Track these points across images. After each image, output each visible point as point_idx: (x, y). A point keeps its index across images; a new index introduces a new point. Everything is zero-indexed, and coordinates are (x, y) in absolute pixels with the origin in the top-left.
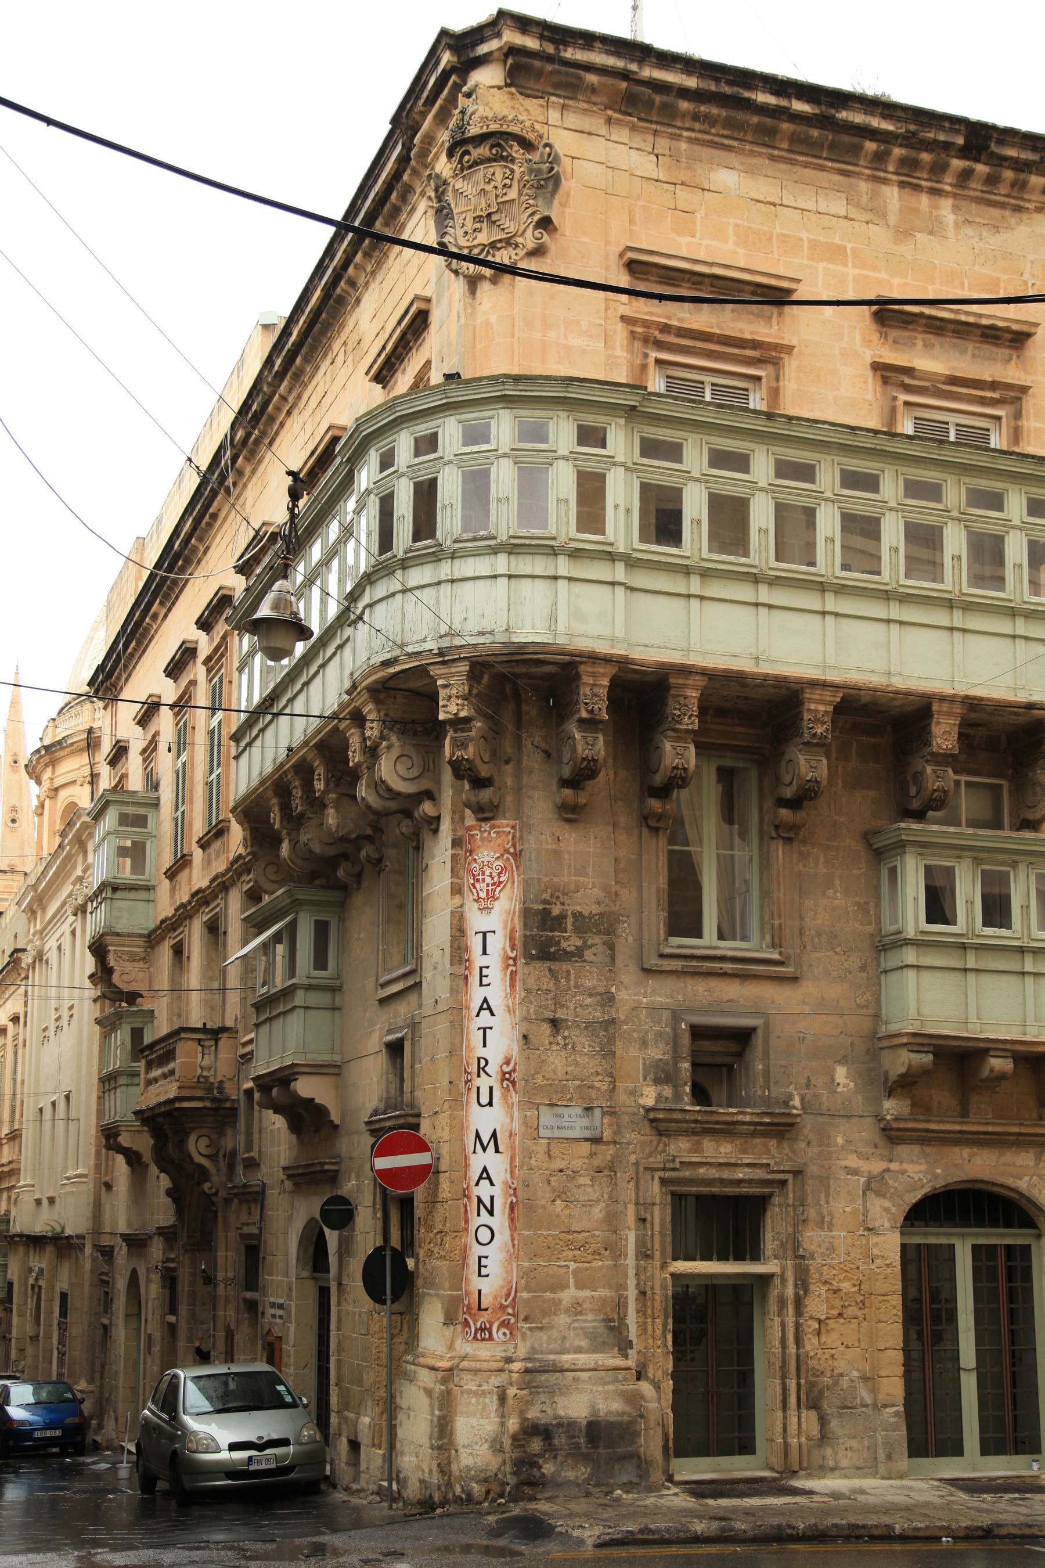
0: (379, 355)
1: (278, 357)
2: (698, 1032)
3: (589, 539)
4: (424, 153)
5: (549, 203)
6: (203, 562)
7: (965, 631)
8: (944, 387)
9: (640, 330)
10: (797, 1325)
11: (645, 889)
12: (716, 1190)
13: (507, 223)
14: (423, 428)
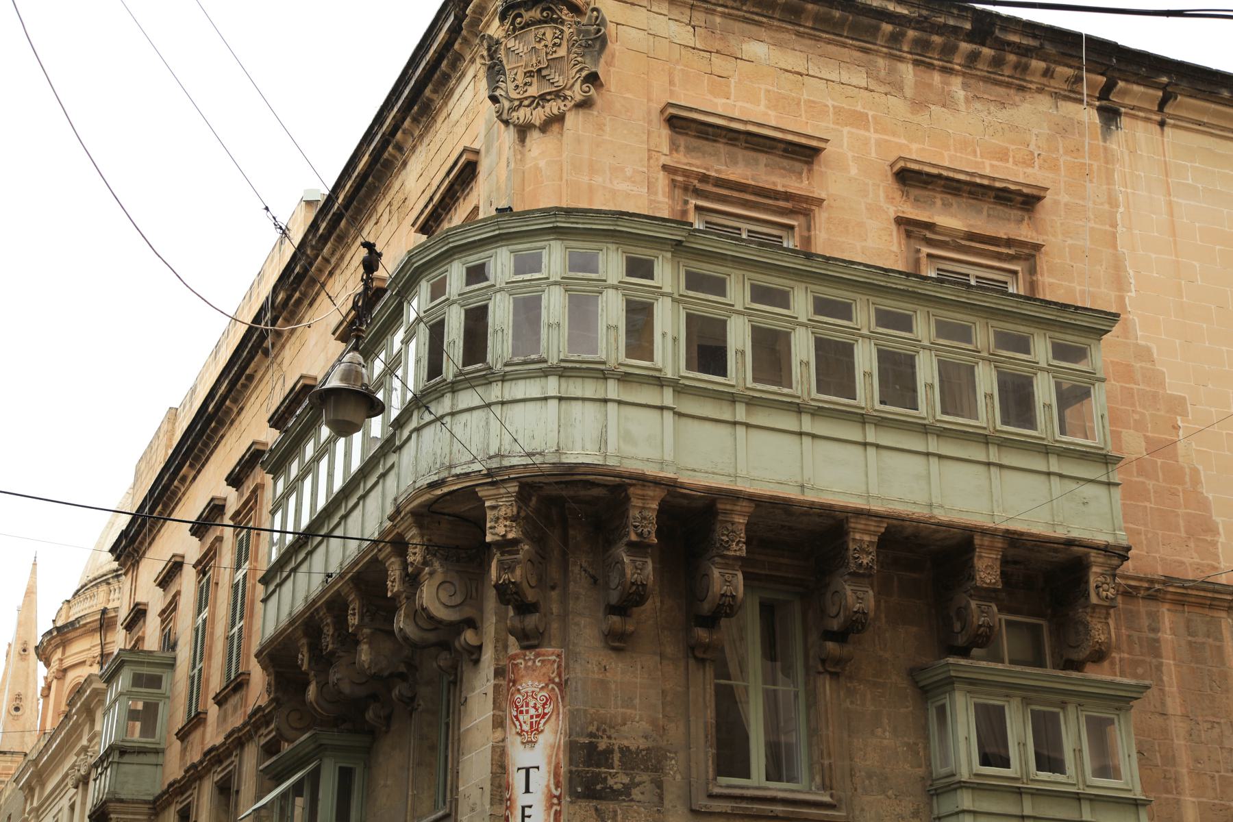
0: (426, 206)
1: (323, 221)
3: (638, 364)
4: (475, 22)
5: (596, 62)
6: (237, 423)
7: (1001, 466)
8: (963, 242)
9: (680, 179)
14: (474, 259)
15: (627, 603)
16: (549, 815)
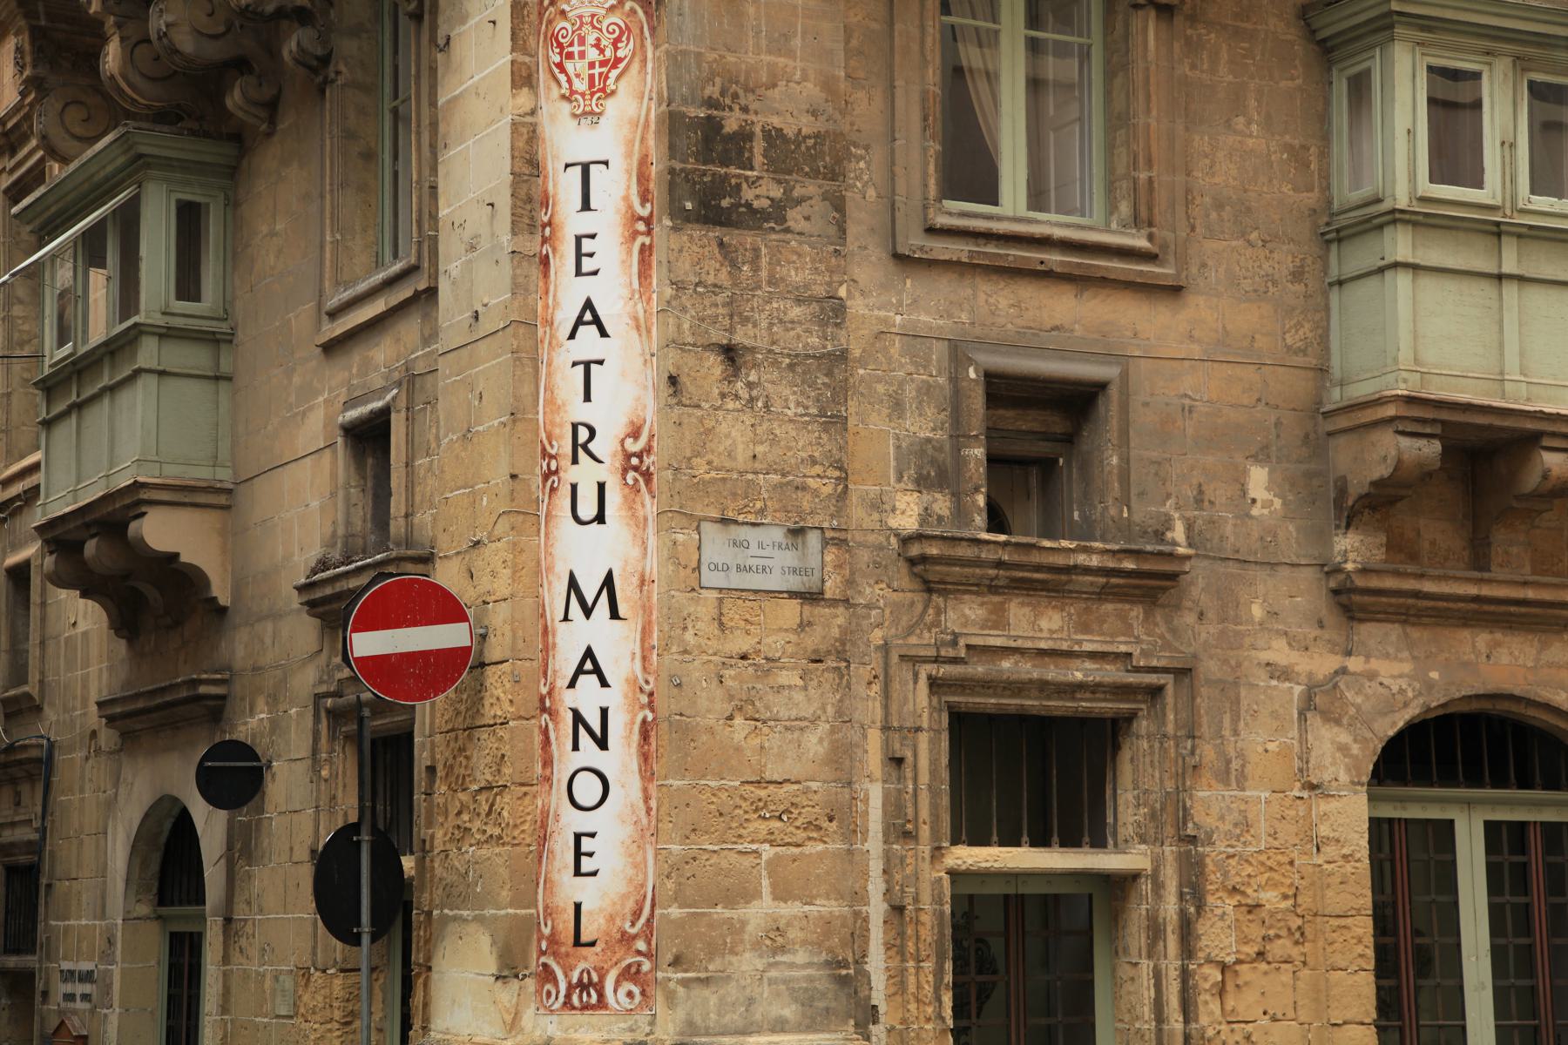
2: (1005, 391)
10: (1185, 975)
11: (899, 93)
12: (1031, 703)
16: (629, 252)
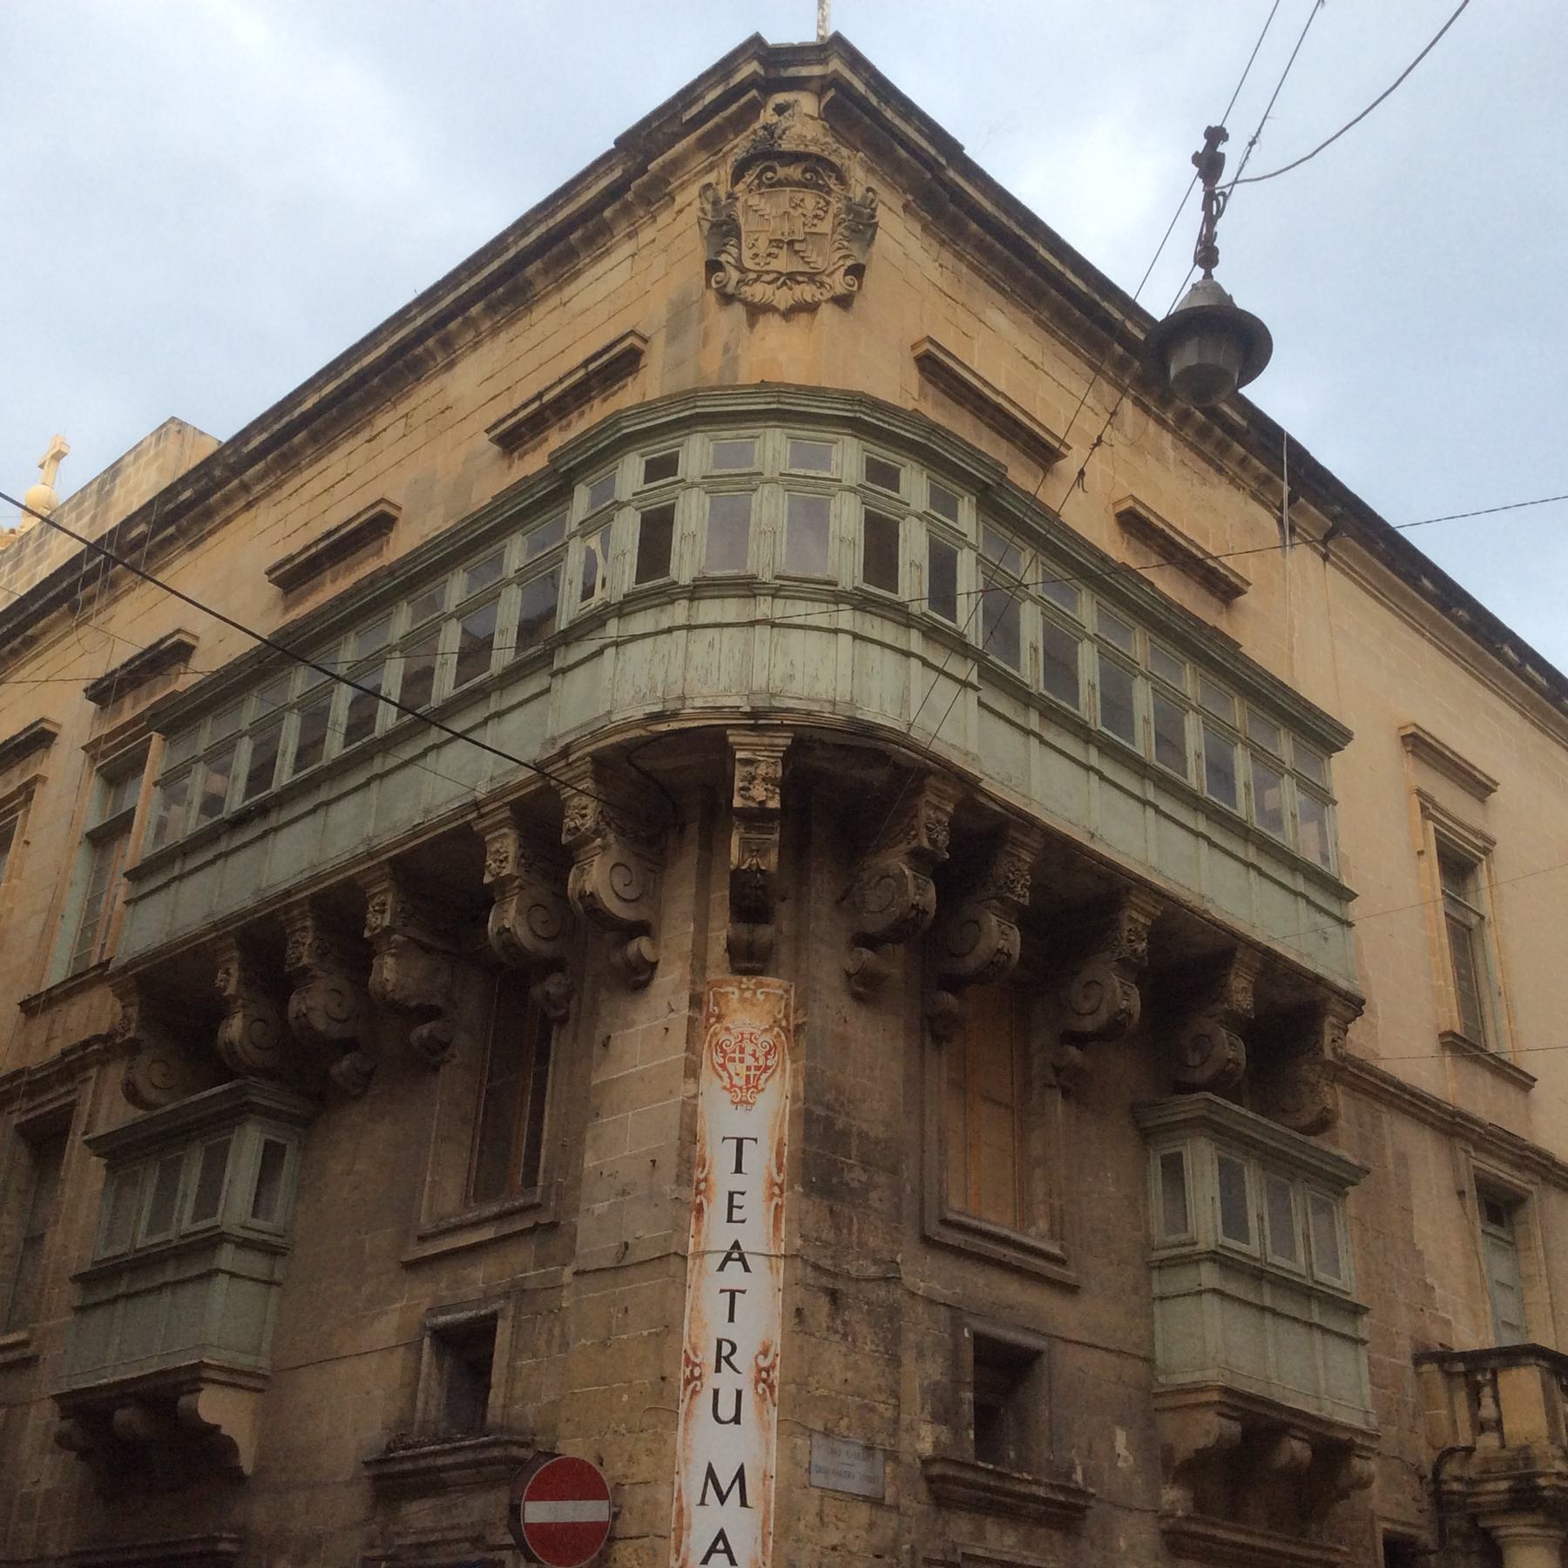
13: (813, 256)
15: (751, 902)
